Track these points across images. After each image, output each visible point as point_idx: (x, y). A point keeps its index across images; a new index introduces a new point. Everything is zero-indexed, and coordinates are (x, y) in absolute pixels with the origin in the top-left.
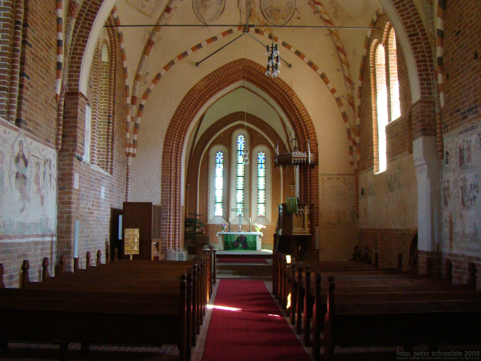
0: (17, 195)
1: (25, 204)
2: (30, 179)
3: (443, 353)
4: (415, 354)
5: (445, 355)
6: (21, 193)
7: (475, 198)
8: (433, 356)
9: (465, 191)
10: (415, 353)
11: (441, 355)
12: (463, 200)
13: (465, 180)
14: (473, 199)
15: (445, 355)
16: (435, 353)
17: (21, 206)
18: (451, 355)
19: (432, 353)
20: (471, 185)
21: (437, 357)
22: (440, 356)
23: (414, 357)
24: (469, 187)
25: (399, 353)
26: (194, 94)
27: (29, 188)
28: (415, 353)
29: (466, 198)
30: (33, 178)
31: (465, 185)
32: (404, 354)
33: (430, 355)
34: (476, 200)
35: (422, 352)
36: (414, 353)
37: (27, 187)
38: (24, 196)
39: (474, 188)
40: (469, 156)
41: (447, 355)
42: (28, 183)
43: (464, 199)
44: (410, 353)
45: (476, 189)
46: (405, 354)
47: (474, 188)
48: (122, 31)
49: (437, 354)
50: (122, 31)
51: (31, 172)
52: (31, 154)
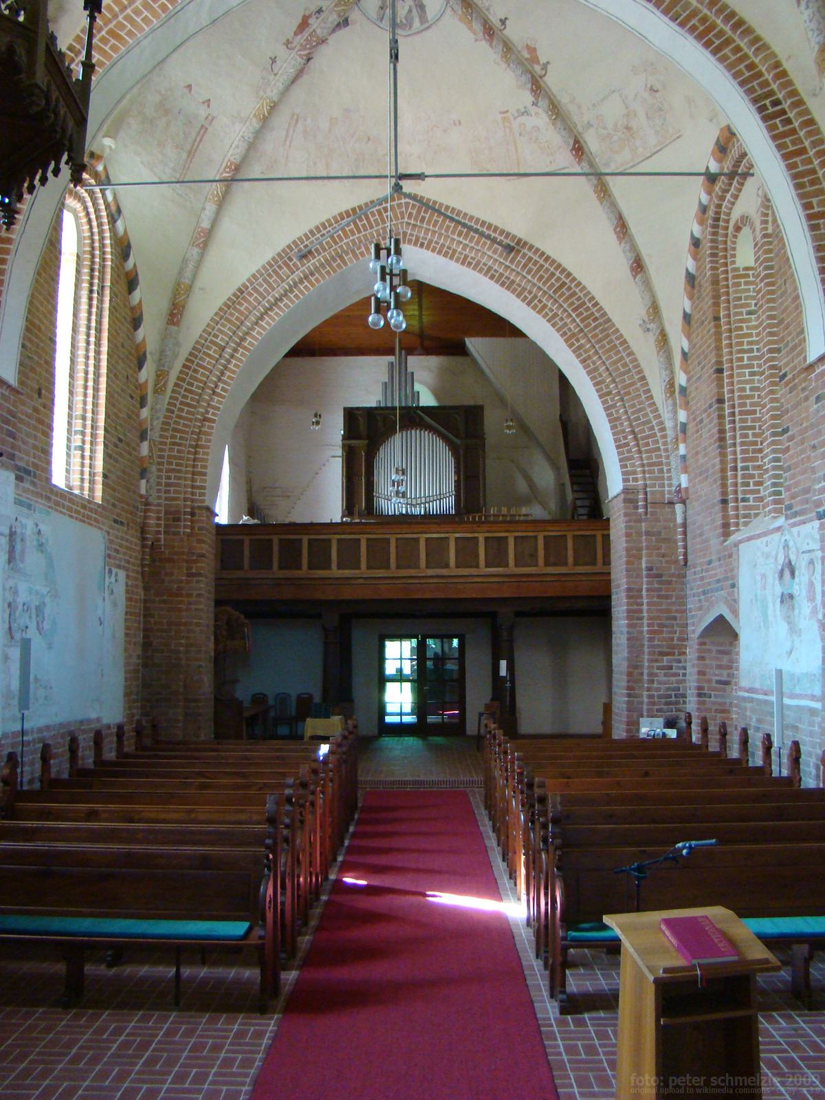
0: (783, 628)
1: (793, 642)
2: (799, 595)
3: (736, 1078)
4: (673, 1082)
5: (741, 1084)
6: (788, 624)
7: (27, 627)
8: (713, 1087)
9: (15, 612)
10: (673, 1080)
11: (732, 1084)
12: (10, 628)
13: (15, 592)
14: (24, 629)
15: (741, 1084)
16: (720, 1079)
17: (788, 645)
18: (698, 1084)
19: (712, 1079)
20: (24, 604)
21: (722, 1087)
22: (730, 1086)
23: (670, 1087)
24: (20, 607)
25: (635, 1080)
26: (649, 458)
27: (800, 613)
28: (673, 1080)
29: (14, 626)
30: (804, 593)
31: (15, 601)
32: (647, 1081)
33: (707, 1083)
34: (28, 630)
35: (688, 1077)
36: (671, 1078)
37: (797, 611)
38: (793, 630)
39: (27, 611)
40: (23, 552)
41: (746, 1084)
42: (796, 605)
43: (12, 626)
44: (662, 1078)
45: (29, 613)
46: (691, 1082)
47: (27, 611)
48: (144, 339)
49: (723, 1081)
50: (144, 339)
51: (800, 584)
52: (801, 551)
